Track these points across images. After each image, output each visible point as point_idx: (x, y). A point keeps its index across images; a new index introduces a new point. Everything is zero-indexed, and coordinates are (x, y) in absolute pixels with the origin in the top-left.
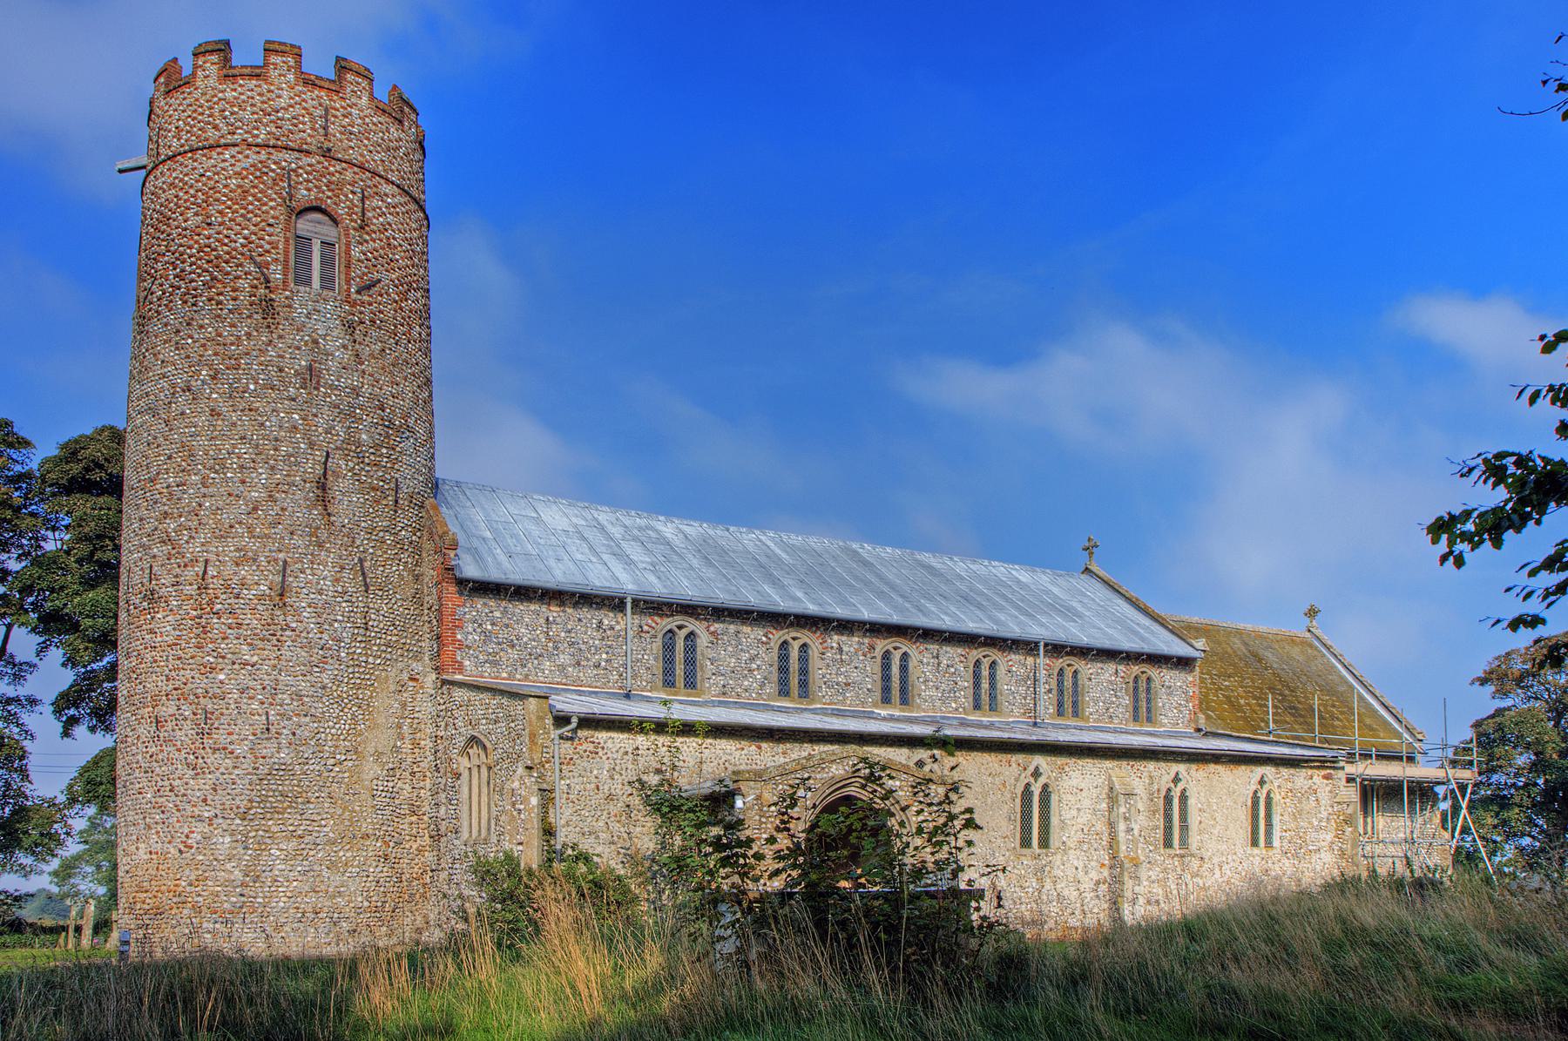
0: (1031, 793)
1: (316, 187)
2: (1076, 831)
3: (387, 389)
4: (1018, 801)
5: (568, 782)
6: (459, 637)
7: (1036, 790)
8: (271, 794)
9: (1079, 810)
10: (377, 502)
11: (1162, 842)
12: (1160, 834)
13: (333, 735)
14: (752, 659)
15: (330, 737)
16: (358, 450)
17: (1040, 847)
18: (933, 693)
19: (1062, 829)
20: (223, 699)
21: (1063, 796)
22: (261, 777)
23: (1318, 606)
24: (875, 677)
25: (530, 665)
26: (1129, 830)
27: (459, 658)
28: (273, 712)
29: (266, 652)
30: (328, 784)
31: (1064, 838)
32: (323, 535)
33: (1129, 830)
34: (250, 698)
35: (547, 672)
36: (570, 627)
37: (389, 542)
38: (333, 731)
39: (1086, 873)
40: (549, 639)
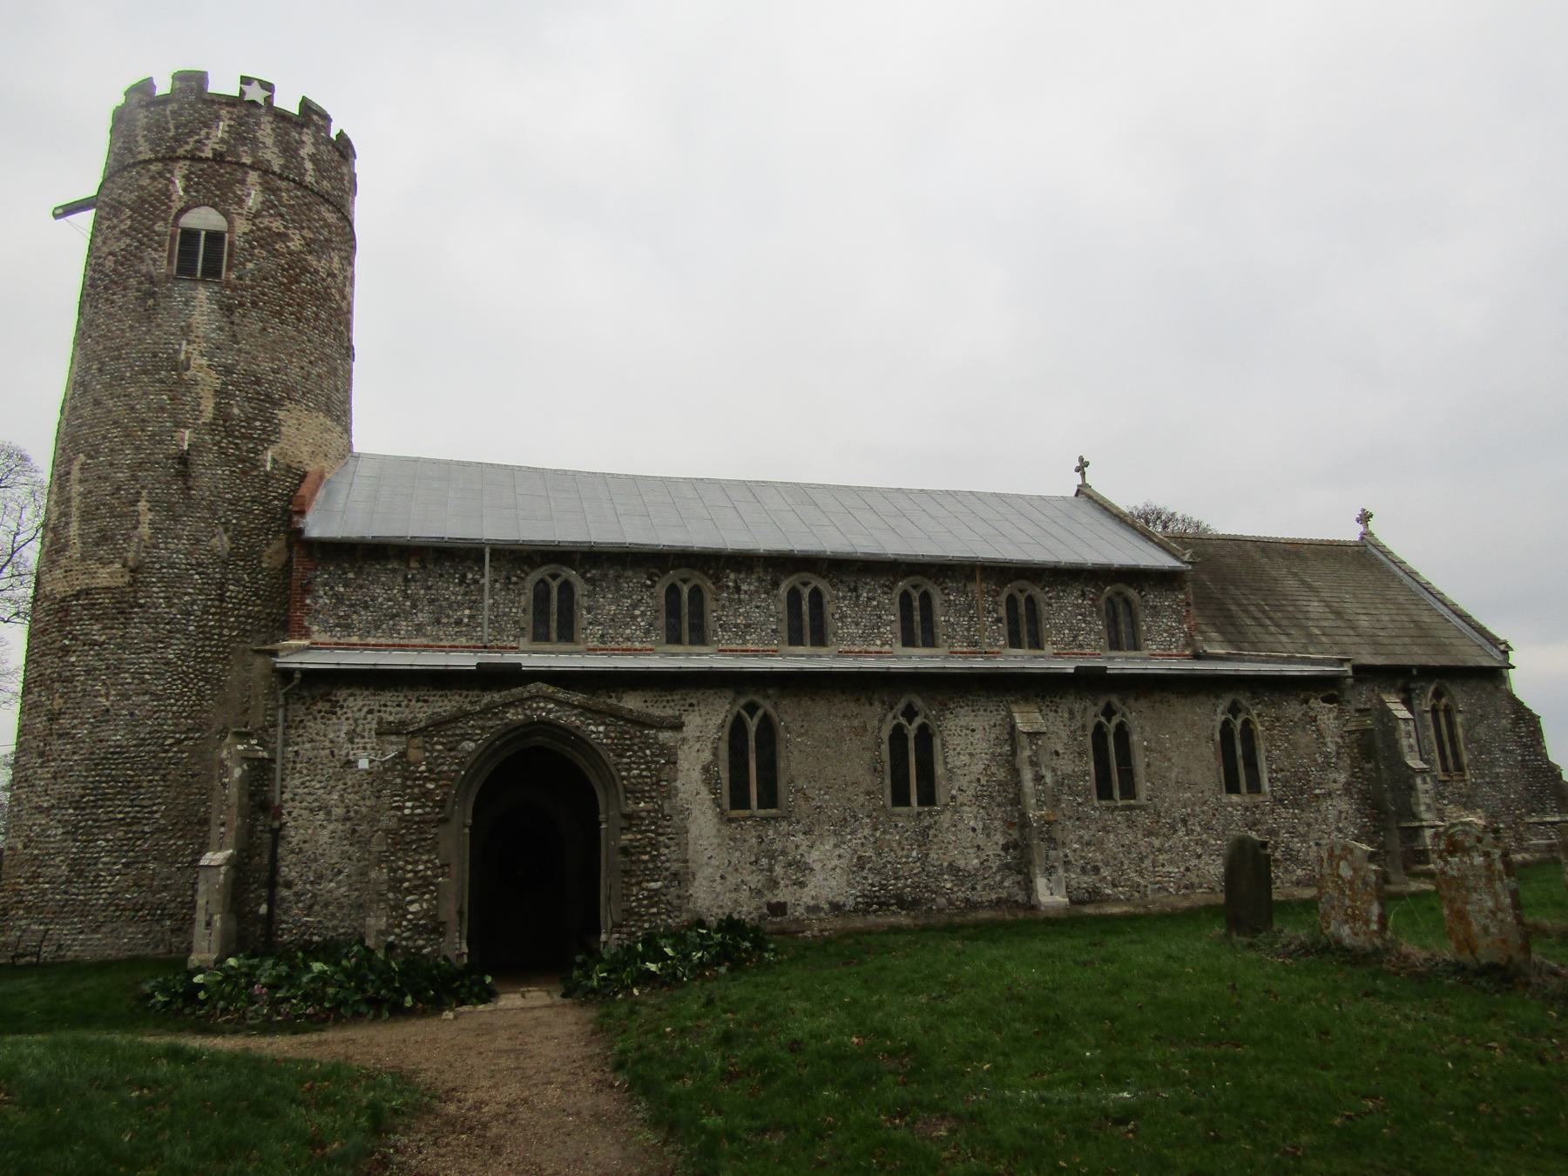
0: (905, 738)
1: (205, 188)
2: (971, 782)
3: (267, 366)
4: (885, 747)
5: (296, 748)
6: (308, 601)
7: (911, 730)
8: (104, 779)
9: (971, 755)
10: (244, 473)
11: (1094, 791)
12: (1091, 780)
13: (174, 713)
14: (635, 606)
15: (170, 715)
16: (227, 424)
17: (920, 803)
18: (853, 630)
19: (950, 779)
20: (71, 682)
21: (948, 739)
22: (96, 761)
23: (1369, 509)
24: (780, 616)
25: (384, 626)
26: (1039, 779)
27: (306, 624)
28: (114, 692)
29: (114, 631)
30: (164, 766)
31: (954, 792)
32: (180, 510)
33: (1039, 779)
34: (95, 680)
35: (402, 632)
36: (430, 584)
37: (256, 512)
38: (175, 708)
39: (988, 836)
40: (406, 597)
